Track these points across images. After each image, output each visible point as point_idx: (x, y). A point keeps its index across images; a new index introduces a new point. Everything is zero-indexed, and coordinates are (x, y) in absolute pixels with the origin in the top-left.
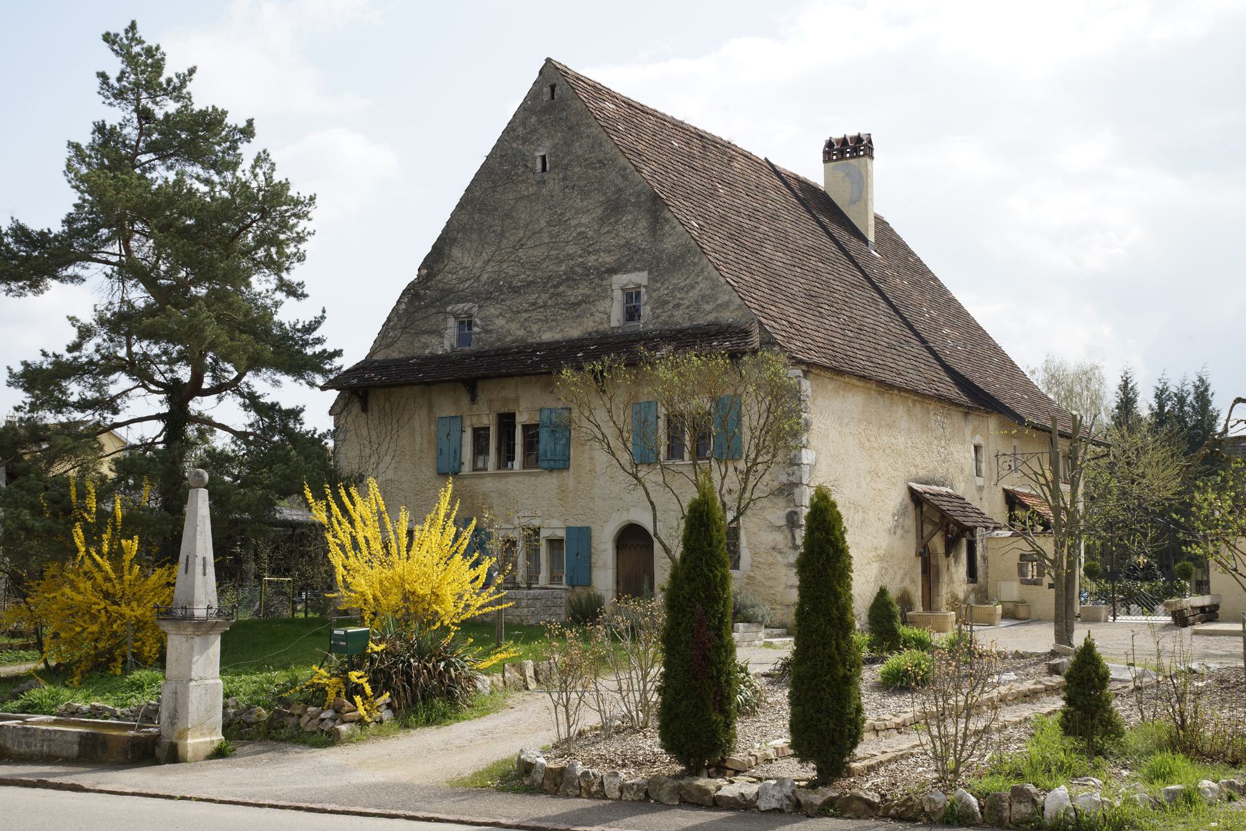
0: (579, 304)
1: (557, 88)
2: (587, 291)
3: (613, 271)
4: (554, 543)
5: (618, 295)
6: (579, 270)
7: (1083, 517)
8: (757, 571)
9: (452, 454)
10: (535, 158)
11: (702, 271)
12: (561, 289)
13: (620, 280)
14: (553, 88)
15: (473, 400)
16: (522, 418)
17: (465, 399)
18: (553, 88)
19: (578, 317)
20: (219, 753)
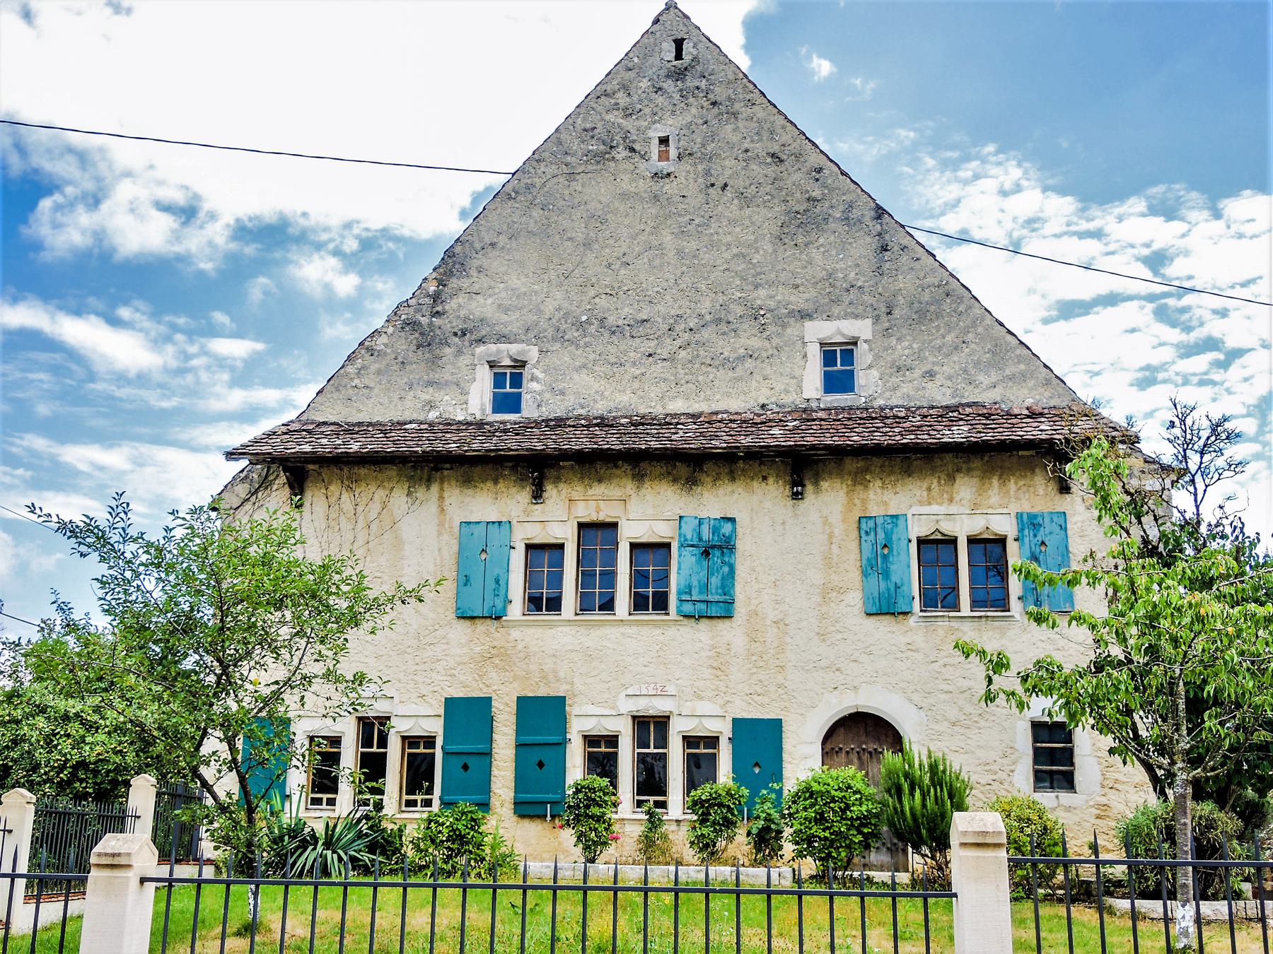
0: (741, 359)
1: (687, 46)
2: (755, 343)
3: (805, 315)
4: (700, 754)
5: (815, 353)
6: (739, 310)
7: (204, 352)
8: (1112, 795)
9: (491, 584)
10: (647, 141)
11: (974, 324)
12: (706, 334)
13: (820, 330)
14: (679, 44)
15: (537, 496)
16: (630, 532)
17: (524, 496)
18: (679, 44)
19: (738, 379)
20: (1144, 215)
